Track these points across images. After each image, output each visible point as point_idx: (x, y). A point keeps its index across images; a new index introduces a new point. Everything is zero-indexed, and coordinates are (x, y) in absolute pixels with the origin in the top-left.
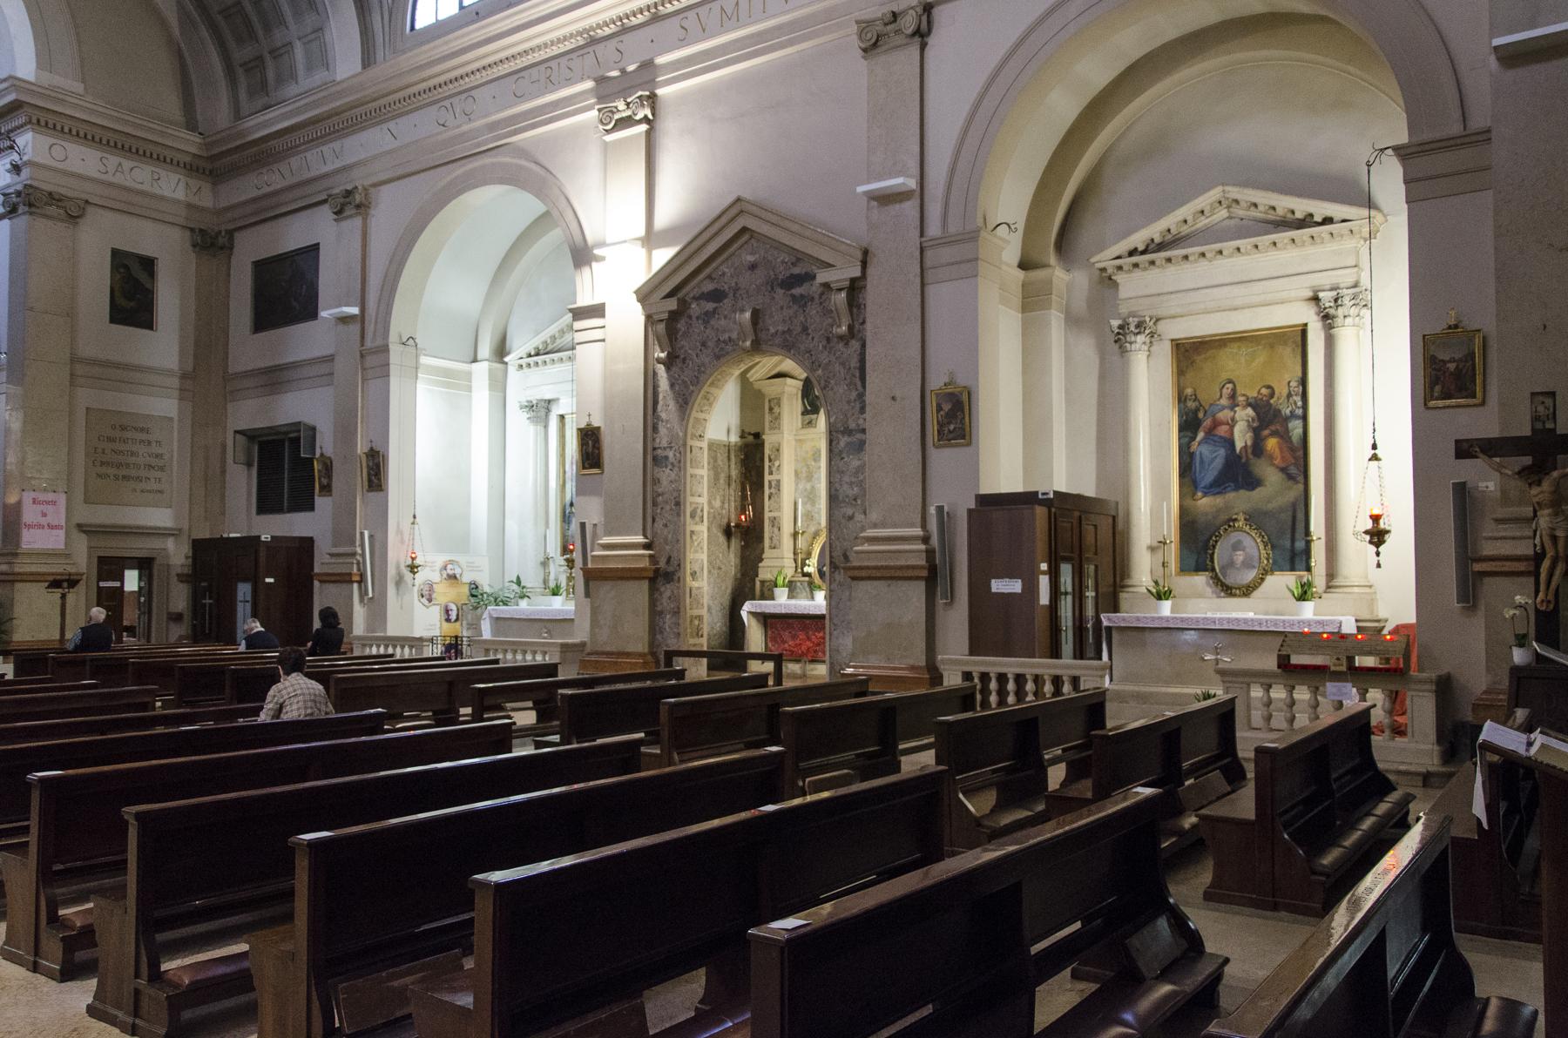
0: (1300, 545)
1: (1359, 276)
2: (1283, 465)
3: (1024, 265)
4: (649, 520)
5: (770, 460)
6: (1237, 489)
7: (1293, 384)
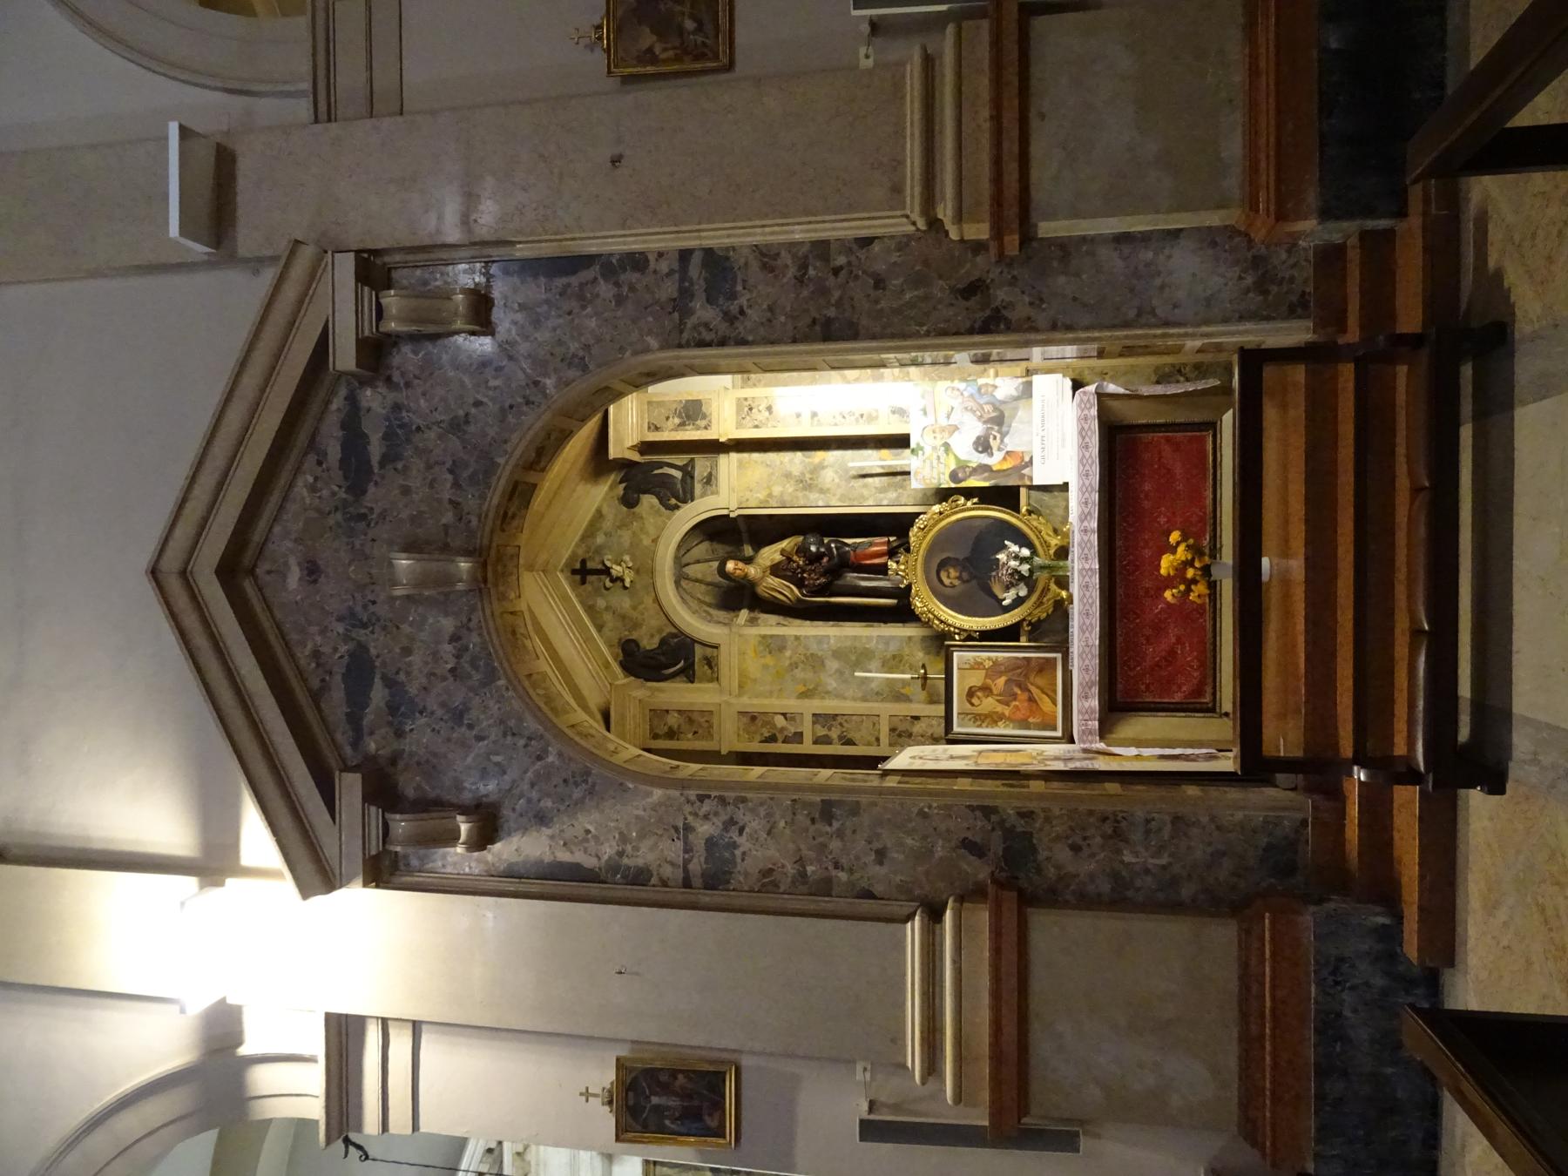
4: (867, 905)
5: (772, 739)
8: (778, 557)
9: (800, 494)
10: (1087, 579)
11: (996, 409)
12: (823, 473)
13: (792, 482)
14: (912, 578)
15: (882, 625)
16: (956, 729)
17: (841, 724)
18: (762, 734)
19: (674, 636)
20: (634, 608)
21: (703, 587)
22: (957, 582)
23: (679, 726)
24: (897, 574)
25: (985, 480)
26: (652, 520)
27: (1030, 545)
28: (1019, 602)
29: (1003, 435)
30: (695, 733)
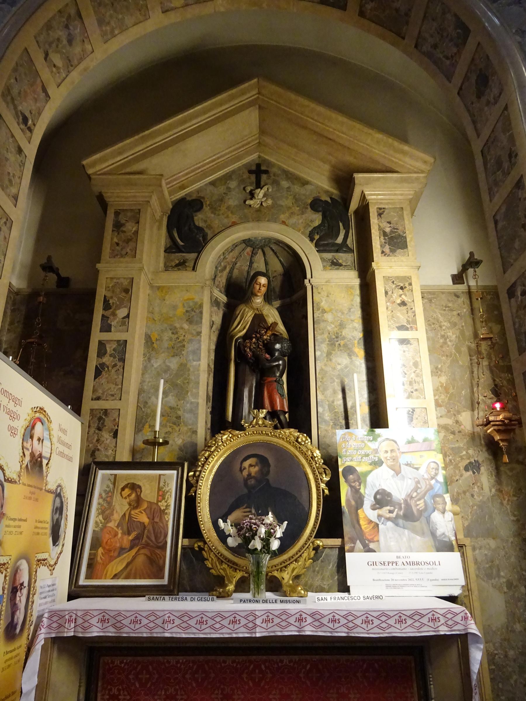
5: (107, 306)
8: (270, 320)
9: (326, 336)
10: (243, 622)
11: (421, 512)
12: (345, 355)
13: (336, 329)
14: (250, 430)
15: (209, 410)
16: (101, 473)
17: (115, 365)
18: (112, 297)
19: (205, 236)
20: (228, 208)
21: (246, 268)
22: (245, 473)
23: (124, 232)
24: (254, 418)
25: (348, 501)
26: (301, 221)
27: (282, 550)
28: (223, 536)
29: (394, 520)
30: (118, 244)
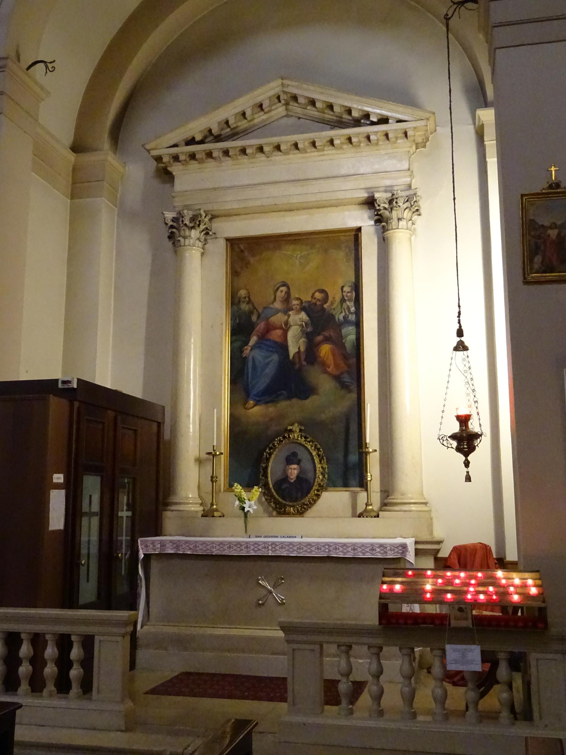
0: (353, 458)
1: (411, 181)
2: (336, 373)
3: (76, 148)
6: (289, 398)
7: (346, 289)
